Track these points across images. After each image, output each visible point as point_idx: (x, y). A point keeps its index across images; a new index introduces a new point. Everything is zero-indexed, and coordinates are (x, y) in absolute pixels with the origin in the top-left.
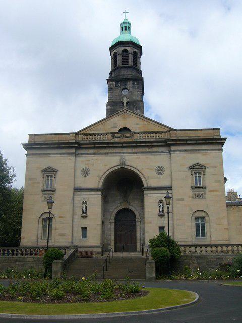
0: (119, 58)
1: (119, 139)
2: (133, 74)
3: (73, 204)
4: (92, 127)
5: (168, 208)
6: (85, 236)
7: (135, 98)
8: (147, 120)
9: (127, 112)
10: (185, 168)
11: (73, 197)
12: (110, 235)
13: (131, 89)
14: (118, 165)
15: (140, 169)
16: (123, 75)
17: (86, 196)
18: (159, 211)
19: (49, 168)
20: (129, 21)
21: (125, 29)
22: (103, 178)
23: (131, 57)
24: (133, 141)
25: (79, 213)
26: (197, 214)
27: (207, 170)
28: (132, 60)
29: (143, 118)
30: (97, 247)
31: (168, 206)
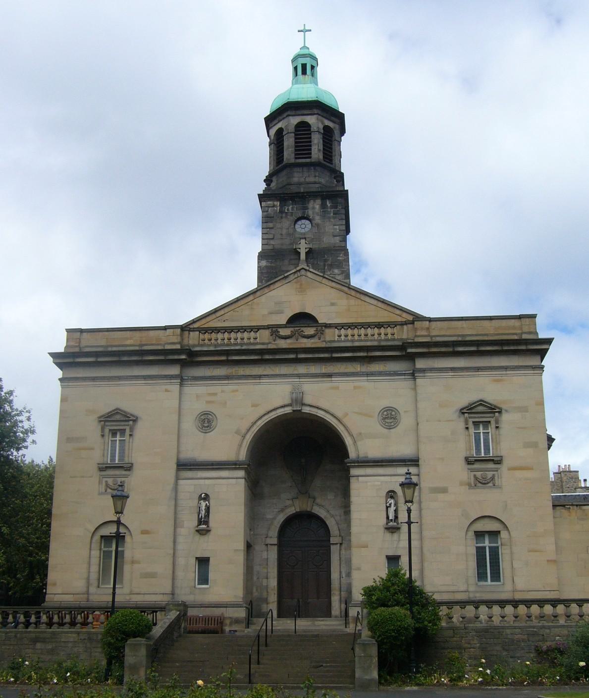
0: (289, 142)
1: (288, 341)
2: (323, 181)
3: (176, 499)
4: (222, 312)
6: (204, 579)
7: (329, 240)
8: (358, 295)
10: (451, 412)
11: (176, 484)
13: (317, 220)
15: (339, 414)
16: (300, 184)
17: (207, 482)
18: (388, 517)
19: (117, 411)
20: (313, 50)
21: (304, 72)
22: (249, 437)
23: (317, 141)
24: (323, 345)
25: (190, 522)
26: (481, 526)
27: (505, 417)
28: (321, 147)
29: (346, 289)
31: (409, 504)
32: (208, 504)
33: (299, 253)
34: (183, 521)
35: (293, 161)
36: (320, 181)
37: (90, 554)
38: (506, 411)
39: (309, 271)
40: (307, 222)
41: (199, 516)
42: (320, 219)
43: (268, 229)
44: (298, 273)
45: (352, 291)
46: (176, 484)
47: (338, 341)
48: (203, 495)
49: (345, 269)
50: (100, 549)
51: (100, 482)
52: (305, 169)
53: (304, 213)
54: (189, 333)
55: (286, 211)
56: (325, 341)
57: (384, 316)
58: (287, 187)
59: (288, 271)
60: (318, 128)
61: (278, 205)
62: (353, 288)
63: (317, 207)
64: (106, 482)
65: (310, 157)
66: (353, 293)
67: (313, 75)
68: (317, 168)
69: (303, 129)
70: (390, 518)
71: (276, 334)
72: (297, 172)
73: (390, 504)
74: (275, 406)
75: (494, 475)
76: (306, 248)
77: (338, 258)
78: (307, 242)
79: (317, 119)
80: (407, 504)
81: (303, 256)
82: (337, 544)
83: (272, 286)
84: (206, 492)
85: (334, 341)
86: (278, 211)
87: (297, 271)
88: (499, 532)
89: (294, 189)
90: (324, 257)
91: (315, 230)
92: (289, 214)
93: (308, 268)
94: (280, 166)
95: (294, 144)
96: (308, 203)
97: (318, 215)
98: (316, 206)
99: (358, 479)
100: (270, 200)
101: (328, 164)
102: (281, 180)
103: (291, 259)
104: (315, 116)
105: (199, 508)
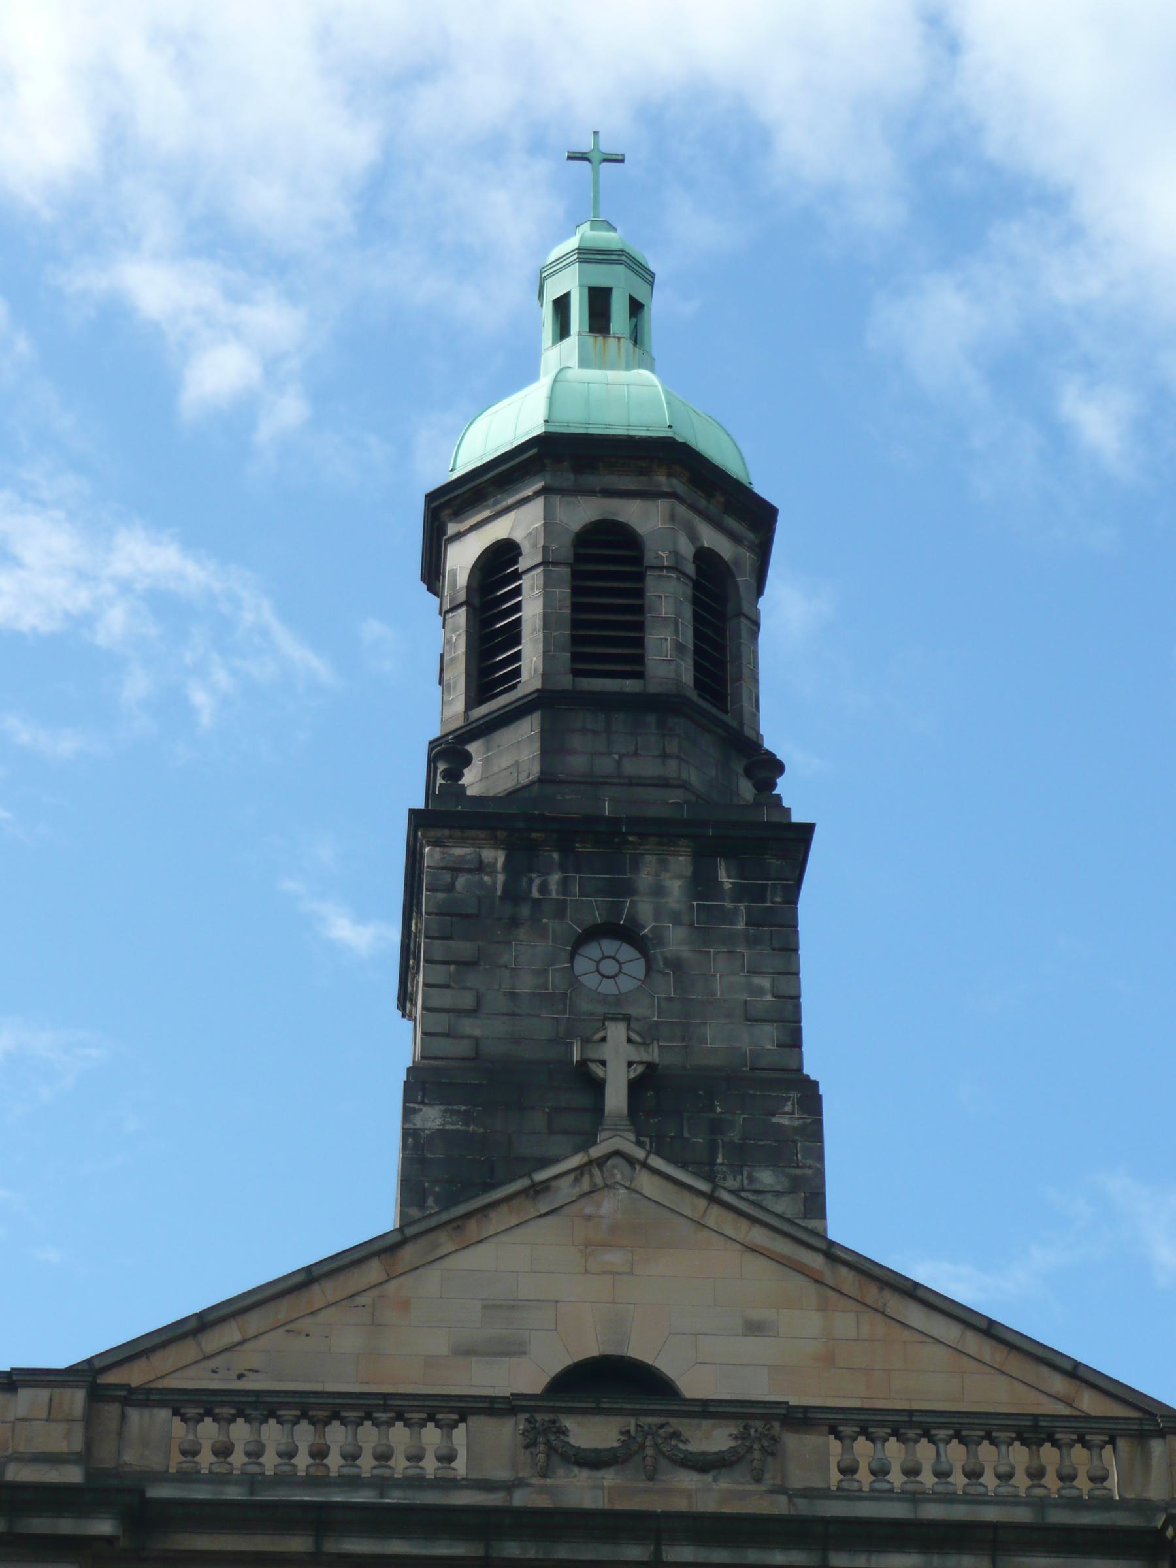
1: (609, 1477)
2: (693, 777)
4: (230, 1333)
8: (872, 1293)
9: (646, 1183)
16: (595, 782)
24: (779, 1506)
28: (687, 637)
29: (815, 1261)
33: (598, 1086)
36: (684, 776)
39: (645, 1165)
40: (627, 952)
43: (452, 967)
44: (596, 1171)
45: (844, 1271)
47: (843, 1494)
49: (809, 1172)
53: (616, 909)
54: (123, 1416)
55: (535, 894)
56: (783, 1490)
60: (676, 554)
61: (500, 865)
62: (849, 1258)
63: (675, 887)
65: (640, 675)
67: (636, 337)
71: (548, 1443)
72: (584, 731)
77: (774, 1120)
78: (635, 1037)
79: (673, 517)
81: (616, 1098)
83: (472, 1225)
85: (824, 1494)
86: (499, 893)
87: (590, 1163)
90: (712, 1109)
91: (666, 986)
93: (640, 1154)
96: (635, 868)
100: (462, 842)
104: (662, 505)
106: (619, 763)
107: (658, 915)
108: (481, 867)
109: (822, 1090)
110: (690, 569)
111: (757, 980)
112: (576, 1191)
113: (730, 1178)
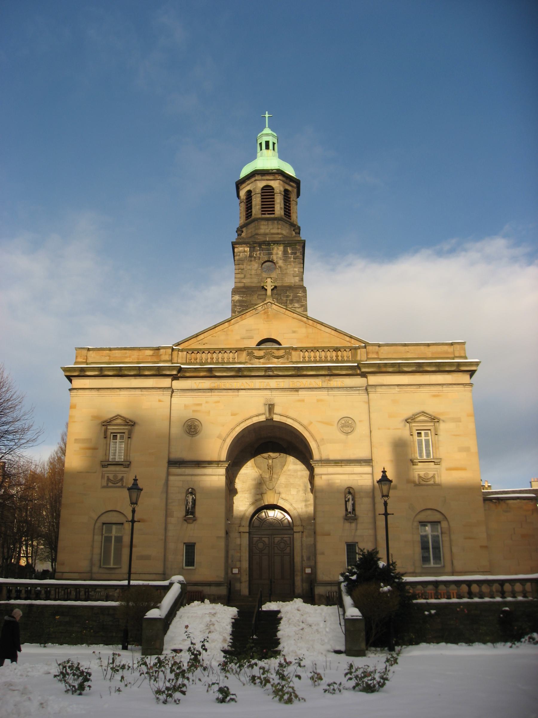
0: (257, 201)
2: (284, 232)
3: (167, 492)
5: (386, 504)
7: (293, 280)
11: (167, 480)
12: (240, 561)
13: (281, 263)
14: (259, 415)
15: (305, 422)
16: (265, 234)
18: (347, 510)
22: (229, 441)
23: (279, 201)
25: (179, 512)
26: (423, 517)
27: (442, 426)
28: (283, 206)
29: (305, 319)
30: (218, 584)
32: (194, 498)
34: (174, 511)
35: (260, 216)
36: (282, 232)
37: (93, 539)
38: (443, 421)
41: (186, 507)
42: (283, 263)
46: (167, 480)
48: (190, 490)
49: (304, 304)
50: (102, 535)
51: (103, 477)
52: (270, 222)
53: (270, 257)
56: (292, 362)
57: (338, 342)
58: (257, 236)
59: (256, 305)
63: (280, 253)
64: (108, 477)
66: (311, 322)
68: (280, 222)
69: (268, 191)
70: (349, 510)
72: (263, 225)
73: (349, 499)
74: (251, 415)
75: (434, 474)
76: (271, 286)
77: (298, 295)
80: (384, 498)
81: (269, 292)
82: (299, 532)
84: (192, 487)
86: (248, 256)
88: (439, 522)
89: (261, 239)
92: (257, 258)
94: (250, 220)
95: (260, 203)
96: (273, 249)
97: (281, 260)
98: (279, 252)
99: (321, 478)
100: (242, 247)
101: (288, 219)
102: (250, 231)
103: (259, 295)
105: (187, 500)
106: (270, 230)
107: (277, 258)
108: (245, 251)
109: (307, 289)
110: (283, 193)
111: (295, 269)
112: (262, 309)
113: (290, 305)
